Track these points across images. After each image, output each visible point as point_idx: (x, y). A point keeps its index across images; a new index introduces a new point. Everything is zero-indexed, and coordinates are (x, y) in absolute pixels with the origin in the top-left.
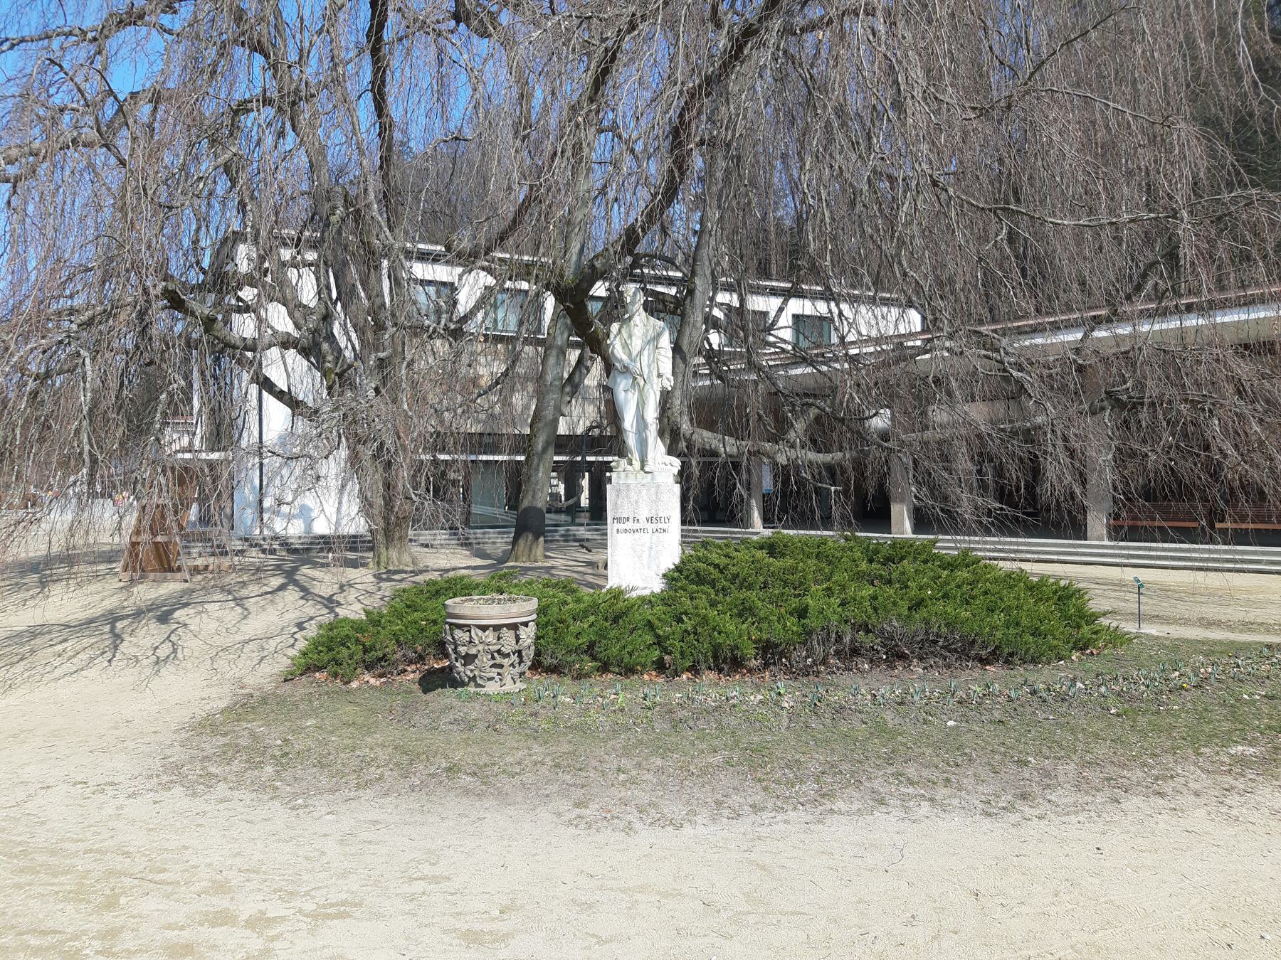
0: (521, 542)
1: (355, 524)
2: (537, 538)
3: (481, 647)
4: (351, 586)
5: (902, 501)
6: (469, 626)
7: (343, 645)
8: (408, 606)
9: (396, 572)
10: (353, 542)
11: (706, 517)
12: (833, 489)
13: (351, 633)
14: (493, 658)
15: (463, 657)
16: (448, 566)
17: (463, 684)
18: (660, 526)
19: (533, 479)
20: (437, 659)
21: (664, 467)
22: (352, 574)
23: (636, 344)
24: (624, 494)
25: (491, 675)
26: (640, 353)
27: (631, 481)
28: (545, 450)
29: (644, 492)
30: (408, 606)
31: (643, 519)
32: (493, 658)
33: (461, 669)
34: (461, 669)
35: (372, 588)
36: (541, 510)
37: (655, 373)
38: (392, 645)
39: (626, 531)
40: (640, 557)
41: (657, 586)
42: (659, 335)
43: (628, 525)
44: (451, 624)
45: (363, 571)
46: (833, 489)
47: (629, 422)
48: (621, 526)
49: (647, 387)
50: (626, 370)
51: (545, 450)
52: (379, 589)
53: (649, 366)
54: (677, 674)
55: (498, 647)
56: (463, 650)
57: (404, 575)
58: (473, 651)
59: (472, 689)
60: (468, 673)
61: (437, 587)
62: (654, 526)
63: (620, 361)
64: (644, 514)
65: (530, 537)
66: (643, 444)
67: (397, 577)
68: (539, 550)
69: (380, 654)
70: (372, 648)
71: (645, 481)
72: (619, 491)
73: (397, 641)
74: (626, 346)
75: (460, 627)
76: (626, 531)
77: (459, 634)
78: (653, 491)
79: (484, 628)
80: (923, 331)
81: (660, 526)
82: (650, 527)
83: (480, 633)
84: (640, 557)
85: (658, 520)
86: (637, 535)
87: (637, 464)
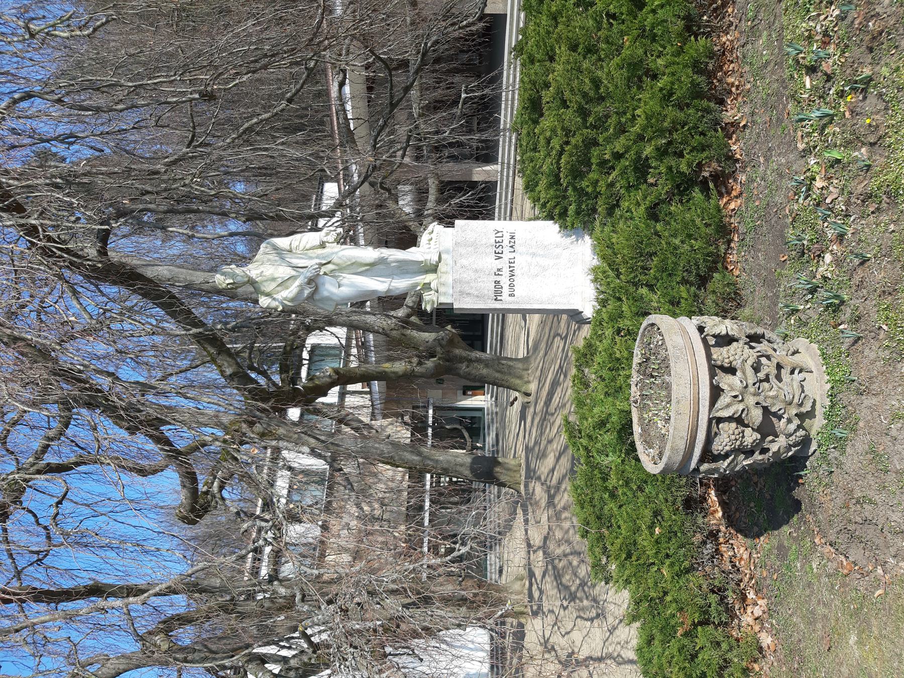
0: (503, 478)
1: (478, 638)
2: (499, 463)
3: (751, 400)
4: (547, 641)
5: (470, 173)
6: (710, 421)
7: (694, 656)
8: (629, 556)
9: (531, 596)
10: (497, 635)
11: (479, 343)
12: (464, 96)
13: (674, 645)
14: (767, 379)
15: (763, 437)
16: (524, 545)
17: (806, 442)
18: (506, 242)
19: (445, 466)
20: (706, 513)
21: (435, 240)
22: (531, 640)
23: (284, 272)
24: (467, 289)
25: (796, 385)
26: (295, 267)
27: (449, 279)
28: (419, 454)
29: (464, 262)
30: (629, 556)
31: (498, 264)
32: (767, 379)
33: (782, 441)
34: (782, 441)
35: (550, 619)
36: (474, 459)
37: (320, 251)
38: (695, 579)
39: (511, 286)
40: (544, 269)
41: (587, 242)
42: (275, 248)
43: (505, 281)
44: (702, 460)
45: (528, 628)
46: (464, 96)
47: (379, 285)
48: (506, 291)
49: (335, 260)
50: (313, 281)
51: (419, 454)
52: (552, 612)
53: (311, 258)
54: (730, 158)
55: (750, 372)
56: (751, 437)
57: (535, 587)
58: (757, 416)
59: (817, 424)
60: (792, 427)
61: (592, 519)
62: (506, 250)
63: (301, 291)
64: (489, 262)
65: (497, 469)
66: (405, 269)
67: (536, 595)
68: (510, 461)
69: (713, 599)
70: (705, 611)
71: (450, 262)
72: (462, 293)
73: (688, 571)
74: (284, 284)
75: (709, 441)
76: (511, 286)
77: (721, 444)
78: (462, 250)
79: (716, 392)
80: (338, 182)
81: (506, 242)
82: (507, 256)
83: (724, 400)
84: (544, 269)
85: (498, 244)
86: (516, 272)
87: (429, 278)
